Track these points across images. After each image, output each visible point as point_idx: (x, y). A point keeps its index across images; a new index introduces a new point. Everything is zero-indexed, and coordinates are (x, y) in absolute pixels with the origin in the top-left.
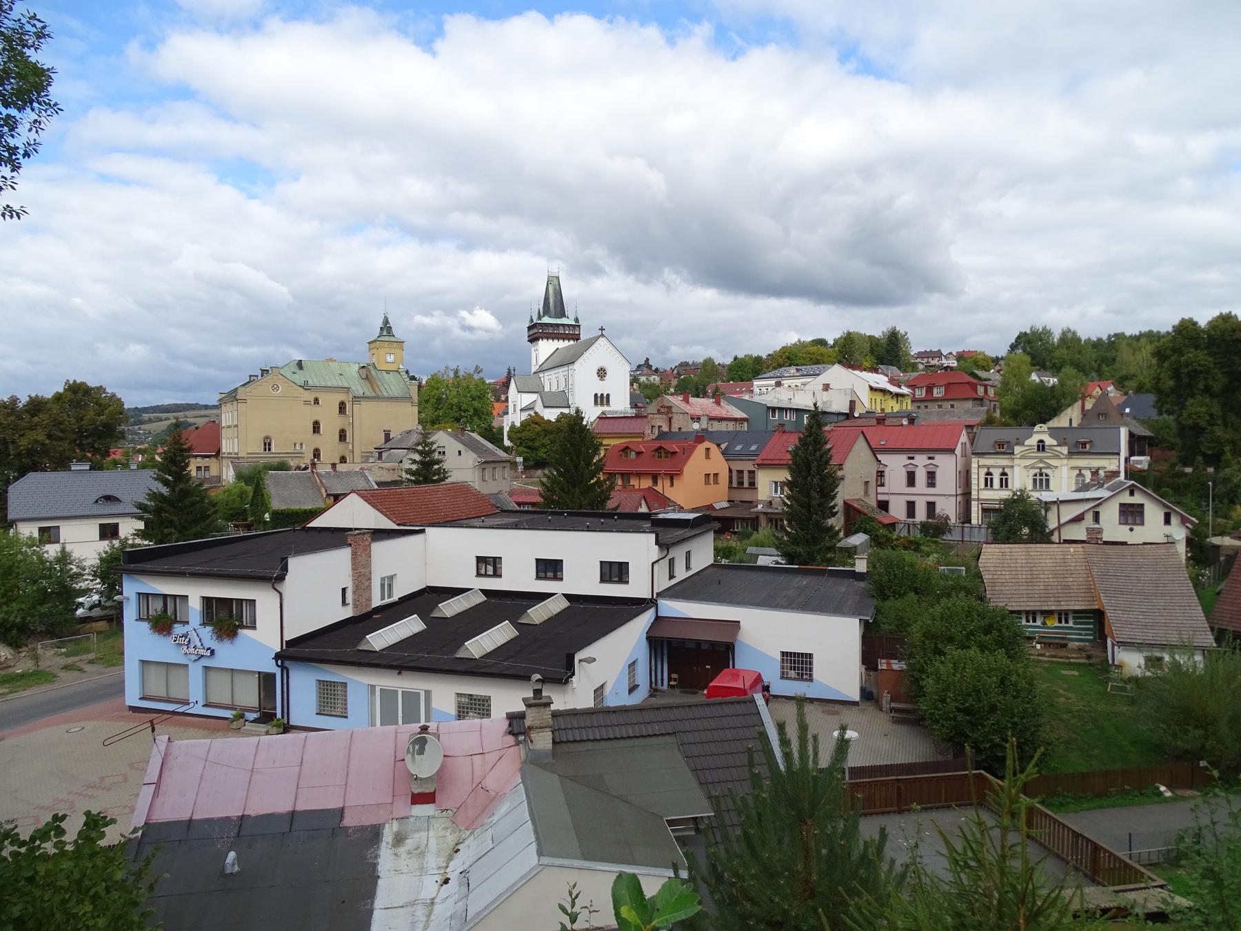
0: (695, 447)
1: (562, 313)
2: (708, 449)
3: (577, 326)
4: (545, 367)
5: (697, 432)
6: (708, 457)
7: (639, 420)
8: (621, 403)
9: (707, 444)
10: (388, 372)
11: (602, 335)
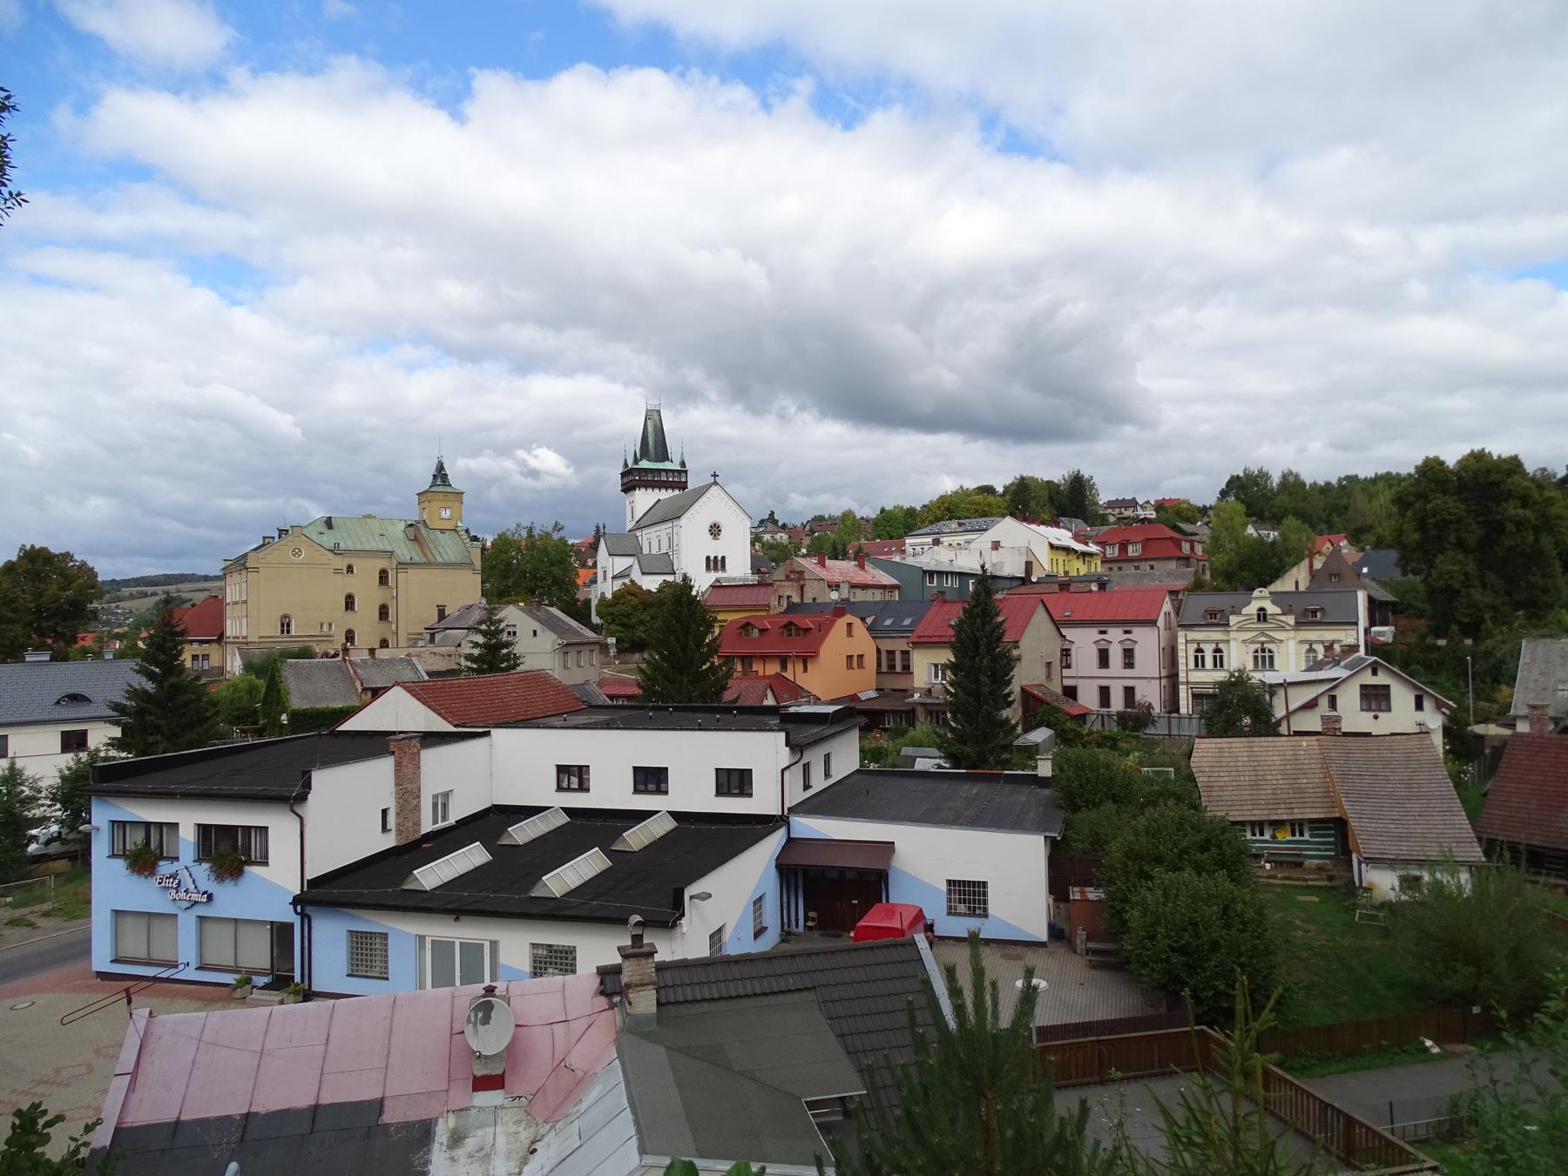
0: (833, 623)
1: (664, 456)
2: (850, 625)
3: (683, 472)
4: (642, 523)
5: (836, 602)
6: (850, 634)
7: (763, 589)
8: (739, 568)
9: (848, 618)
10: (443, 531)
11: (715, 483)
